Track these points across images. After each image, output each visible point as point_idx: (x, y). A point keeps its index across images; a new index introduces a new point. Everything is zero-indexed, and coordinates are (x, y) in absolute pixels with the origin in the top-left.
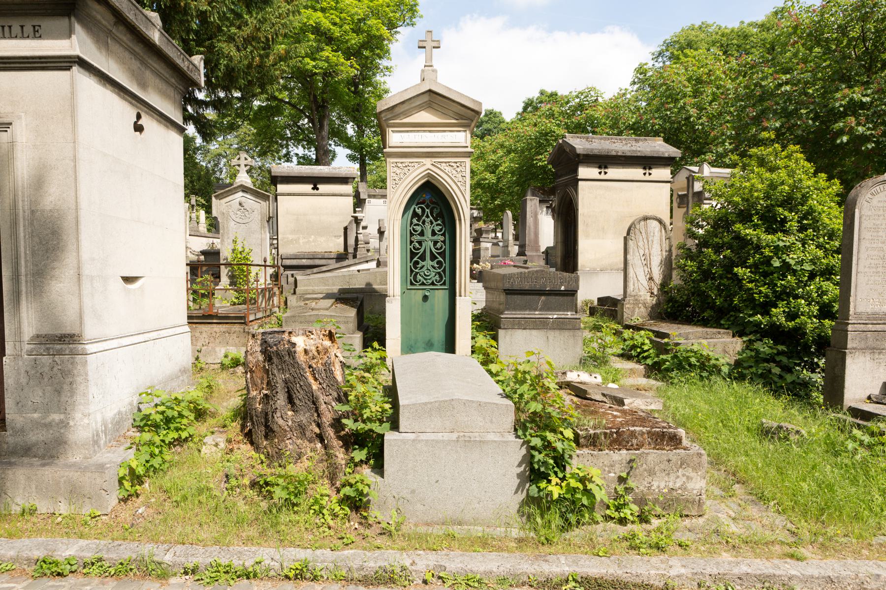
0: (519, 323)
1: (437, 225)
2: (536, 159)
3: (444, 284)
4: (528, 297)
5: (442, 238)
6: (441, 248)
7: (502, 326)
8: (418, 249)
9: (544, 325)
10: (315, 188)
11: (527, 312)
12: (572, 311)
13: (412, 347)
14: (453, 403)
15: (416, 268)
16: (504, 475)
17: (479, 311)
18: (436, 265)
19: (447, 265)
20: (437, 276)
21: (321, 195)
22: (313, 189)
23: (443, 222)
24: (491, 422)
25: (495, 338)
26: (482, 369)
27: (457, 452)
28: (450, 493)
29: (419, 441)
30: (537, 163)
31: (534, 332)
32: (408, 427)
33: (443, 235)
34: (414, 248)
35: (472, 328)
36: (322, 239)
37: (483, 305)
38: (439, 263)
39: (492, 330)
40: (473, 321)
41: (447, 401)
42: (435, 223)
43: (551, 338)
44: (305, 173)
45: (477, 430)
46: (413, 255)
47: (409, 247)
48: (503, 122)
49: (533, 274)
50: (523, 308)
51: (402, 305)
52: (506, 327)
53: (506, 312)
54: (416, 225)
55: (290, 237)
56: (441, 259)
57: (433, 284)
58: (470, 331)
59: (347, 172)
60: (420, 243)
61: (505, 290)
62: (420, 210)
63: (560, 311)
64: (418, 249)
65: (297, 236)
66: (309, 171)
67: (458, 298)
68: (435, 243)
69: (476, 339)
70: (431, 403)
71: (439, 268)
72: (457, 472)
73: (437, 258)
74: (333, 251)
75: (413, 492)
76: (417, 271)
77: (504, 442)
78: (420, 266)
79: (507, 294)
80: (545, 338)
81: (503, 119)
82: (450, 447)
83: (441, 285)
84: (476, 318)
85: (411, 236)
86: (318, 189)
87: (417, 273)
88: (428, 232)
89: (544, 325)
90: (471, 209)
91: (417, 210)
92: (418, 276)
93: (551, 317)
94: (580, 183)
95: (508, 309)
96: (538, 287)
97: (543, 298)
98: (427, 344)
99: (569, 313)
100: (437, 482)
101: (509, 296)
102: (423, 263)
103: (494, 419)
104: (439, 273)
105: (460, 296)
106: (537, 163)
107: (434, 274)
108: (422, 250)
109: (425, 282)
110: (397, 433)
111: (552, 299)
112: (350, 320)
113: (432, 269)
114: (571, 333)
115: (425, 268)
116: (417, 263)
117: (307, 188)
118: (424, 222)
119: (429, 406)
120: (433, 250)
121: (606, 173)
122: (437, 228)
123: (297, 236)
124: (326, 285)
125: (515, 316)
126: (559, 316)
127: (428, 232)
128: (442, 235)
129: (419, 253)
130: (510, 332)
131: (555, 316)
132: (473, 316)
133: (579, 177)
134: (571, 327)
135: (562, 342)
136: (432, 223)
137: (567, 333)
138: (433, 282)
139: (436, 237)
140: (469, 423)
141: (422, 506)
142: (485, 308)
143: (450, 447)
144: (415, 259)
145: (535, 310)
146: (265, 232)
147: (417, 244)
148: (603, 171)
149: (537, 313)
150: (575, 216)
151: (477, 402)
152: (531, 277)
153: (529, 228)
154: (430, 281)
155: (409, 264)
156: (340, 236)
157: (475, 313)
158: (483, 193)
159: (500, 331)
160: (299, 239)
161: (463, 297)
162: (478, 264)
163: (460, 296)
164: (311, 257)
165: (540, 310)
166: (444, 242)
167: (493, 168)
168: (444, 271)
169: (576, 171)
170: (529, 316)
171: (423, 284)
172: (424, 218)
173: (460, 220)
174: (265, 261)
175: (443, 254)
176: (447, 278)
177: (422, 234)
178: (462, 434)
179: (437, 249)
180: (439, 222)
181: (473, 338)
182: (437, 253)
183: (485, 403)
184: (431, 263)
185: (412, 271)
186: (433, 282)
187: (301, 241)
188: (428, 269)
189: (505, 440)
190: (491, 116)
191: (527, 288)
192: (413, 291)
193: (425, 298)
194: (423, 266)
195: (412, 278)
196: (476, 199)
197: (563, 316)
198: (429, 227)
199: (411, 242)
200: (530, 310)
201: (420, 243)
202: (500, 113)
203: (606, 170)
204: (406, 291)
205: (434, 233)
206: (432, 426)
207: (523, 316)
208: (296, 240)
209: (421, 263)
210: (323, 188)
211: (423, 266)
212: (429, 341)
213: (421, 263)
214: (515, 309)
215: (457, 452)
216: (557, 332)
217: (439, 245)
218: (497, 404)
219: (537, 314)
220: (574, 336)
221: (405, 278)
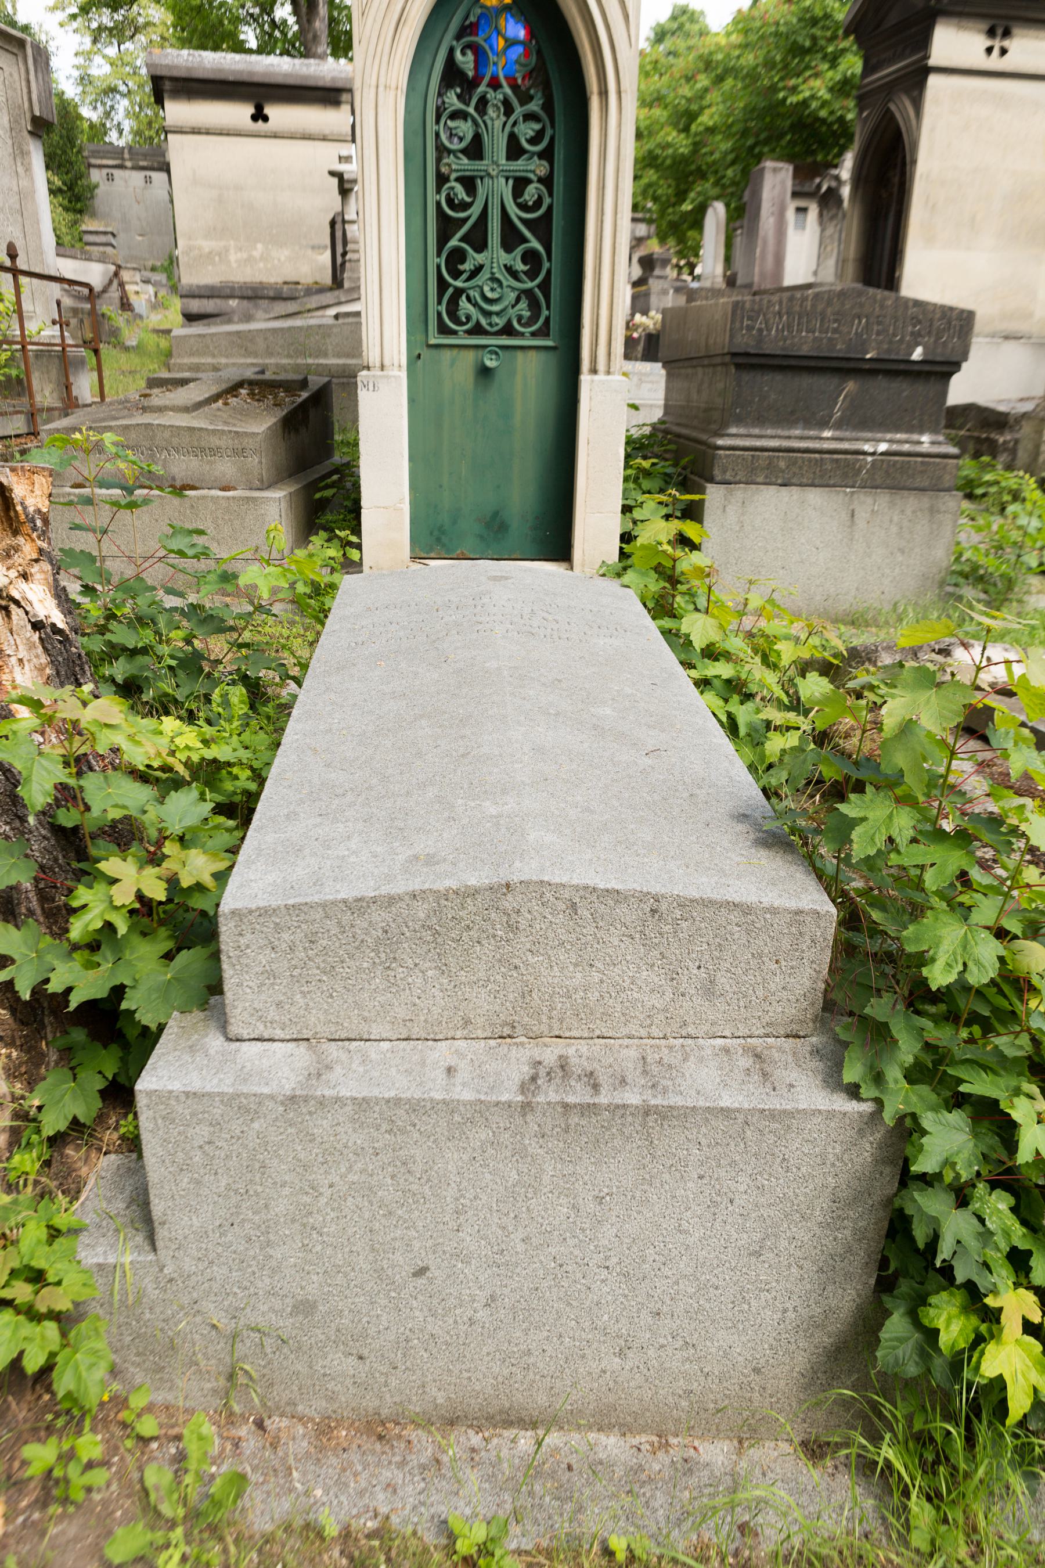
0: (771, 466)
1: (529, 117)
2: (784, 88)
3: (544, 332)
4: (806, 381)
5: (541, 168)
6: (538, 203)
7: (103, 339)
8: (465, 206)
9: (845, 475)
10: (259, 116)
11: (797, 432)
12: (934, 431)
13: (442, 530)
14: (509, 902)
15: (456, 274)
16: (757, 1254)
17: (647, 430)
18: (520, 267)
19: (554, 265)
20: (523, 305)
21: (275, 136)
22: (255, 118)
23: (548, 106)
24: (709, 990)
25: (693, 512)
26: (651, 628)
27: (520, 1153)
28: (482, 1314)
29: (322, 1102)
30: (785, 99)
31: (815, 497)
32: (272, 1014)
33: (547, 155)
34: (450, 201)
35: (626, 479)
36: (283, 254)
37: (657, 414)
38: (530, 257)
39: (685, 486)
40: (628, 457)
41: (474, 893)
42: (519, 111)
43: (862, 515)
44: (233, 72)
45: (633, 1028)
46: (446, 227)
47: (432, 197)
48: (708, 34)
49: (829, 303)
50: (786, 418)
51: (412, 401)
52: (728, 476)
53: (733, 430)
54: (455, 115)
55: (207, 245)
56: (535, 244)
57: (508, 330)
58: (619, 486)
59: (336, 74)
60: (469, 183)
61: (734, 355)
62: (470, 56)
63: (897, 429)
64: (465, 206)
65: (222, 243)
66: (241, 67)
67: (585, 379)
68: (520, 184)
69: (637, 514)
70: (392, 900)
71: (532, 275)
72: (520, 1234)
73: (525, 240)
74: (302, 281)
75: (305, 1308)
76: (459, 284)
77: (773, 1115)
78: (468, 266)
79: (738, 366)
80: (845, 516)
81: (706, 26)
82: (484, 1134)
83: (533, 334)
84: (635, 447)
85: (439, 160)
86: (266, 119)
87: (459, 292)
88: (497, 145)
89: (845, 475)
90: (634, 220)
91: (458, 55)
92: (463, 303)
93: (867, 447)
94: (934, 81)
95: (739, 421)
96: (840, 348)
97: (851, 386)
98: (488, 525)
99: (925, 438)
100: (421, 1272)
101: (746, 377)
102: (480, 258)
103: (723, 980)
104: (528, 293)
105: (594, 371)
106: (785, 99)
107: (513, 296)
108: (475, 211)
109: (483, 322)
110: (215, 1042)
111: (881, 388)
112: (250, 443)
113: (508, 281)
114: (925, 500)
115: (485, 275)
116: (456, 257)
117: (240, 113)
118: (482, 104)
119: (378, 916)
120: (513, 210)
121: (1004, 52)
122: (526, 131)
123: (222, 243)
124: (248, 353)
125: (759, 443)
126: (895, 447)
127: (497, 145)
128: (541, 155)
129: (465, 220)
130: (740, 492)
131: (883, 447)
132: (629, 442)
133: (932, 62)
134: (926, 483)
135: (894, 529)
136: (509, 110)
137: (912, 502)
138: (509, 323)
139: (520, 165)
140: (593, 996)
141: (352, 1361)
142: (661, 422)
143: (484, 1134)
144: (454, 242)
145: (824, 424)
146: (28, 169)
147: (459, 189)
148: (997, 44)
149: (827, 434)
150: (903, 173)
151: (642, 897)
152: (823, 314)
153: (765, 242)
154: (500, 322)
155: (433, 260)
156: (326, 247)
157: (636, 433)
158: (659, 178)
159: (710, 488)
160: (227, 250)
161: (601, 377)
162: (645, 312)
163: (594, 371)
164: (250, 293)
165: (838, 426)
166: (547, 181)
167: (685, 119)
168: (545, 287)
169: (924, 41)
170: (803, 445)
171: (478, 330)
172: (482, 88)
173: (604, 93)
174: (13, 255)
175: (542, 227)
176: (553, 312)
177: (475, 149)
178: (550, 1055)
179: (524, 207)
180: (534, 106)
181: (626, 509)
182: (524, 221)
183: (685, 904)
184: (504, 258)
185: (442, 285)
186: (509, 323)
187: (233, 257)
188: (493, 279)
189: (775, 1103)
190: (685, 18)
191: (805, 350)
192: (447, 354)
193: (484, 372)
194: (478, 270)
195: (443, 308)
196: (644, 192)
197: (906, 447)
198: (498, 124)
199: (442, 179)
200: (808, 424)
201: (469, 183)
202: (702, 13)
203: (1006, 43)
204: (426, 353)
205: (515, 150)
206: (402, 1012)
207: (786, 444)
208: (220, 255)
209: (474, 258)
210: (279, 114)
211: (478, 270)
212: (496, 514)
213: (474, 258)
214: (760, 420)
215: (520, 1153)
216: (882, 500)
217: (531, 193)
218: (745, 909)
219: (827, 438)
220: (933, 511)
221: (419, 308)
